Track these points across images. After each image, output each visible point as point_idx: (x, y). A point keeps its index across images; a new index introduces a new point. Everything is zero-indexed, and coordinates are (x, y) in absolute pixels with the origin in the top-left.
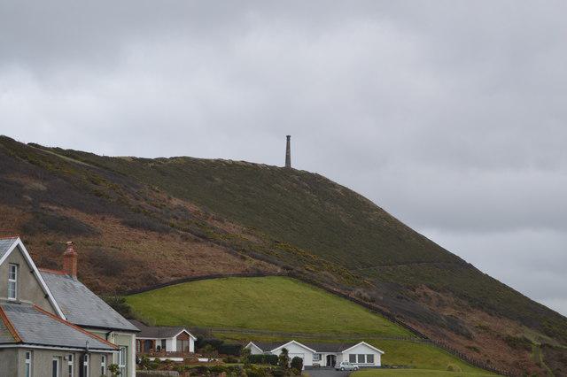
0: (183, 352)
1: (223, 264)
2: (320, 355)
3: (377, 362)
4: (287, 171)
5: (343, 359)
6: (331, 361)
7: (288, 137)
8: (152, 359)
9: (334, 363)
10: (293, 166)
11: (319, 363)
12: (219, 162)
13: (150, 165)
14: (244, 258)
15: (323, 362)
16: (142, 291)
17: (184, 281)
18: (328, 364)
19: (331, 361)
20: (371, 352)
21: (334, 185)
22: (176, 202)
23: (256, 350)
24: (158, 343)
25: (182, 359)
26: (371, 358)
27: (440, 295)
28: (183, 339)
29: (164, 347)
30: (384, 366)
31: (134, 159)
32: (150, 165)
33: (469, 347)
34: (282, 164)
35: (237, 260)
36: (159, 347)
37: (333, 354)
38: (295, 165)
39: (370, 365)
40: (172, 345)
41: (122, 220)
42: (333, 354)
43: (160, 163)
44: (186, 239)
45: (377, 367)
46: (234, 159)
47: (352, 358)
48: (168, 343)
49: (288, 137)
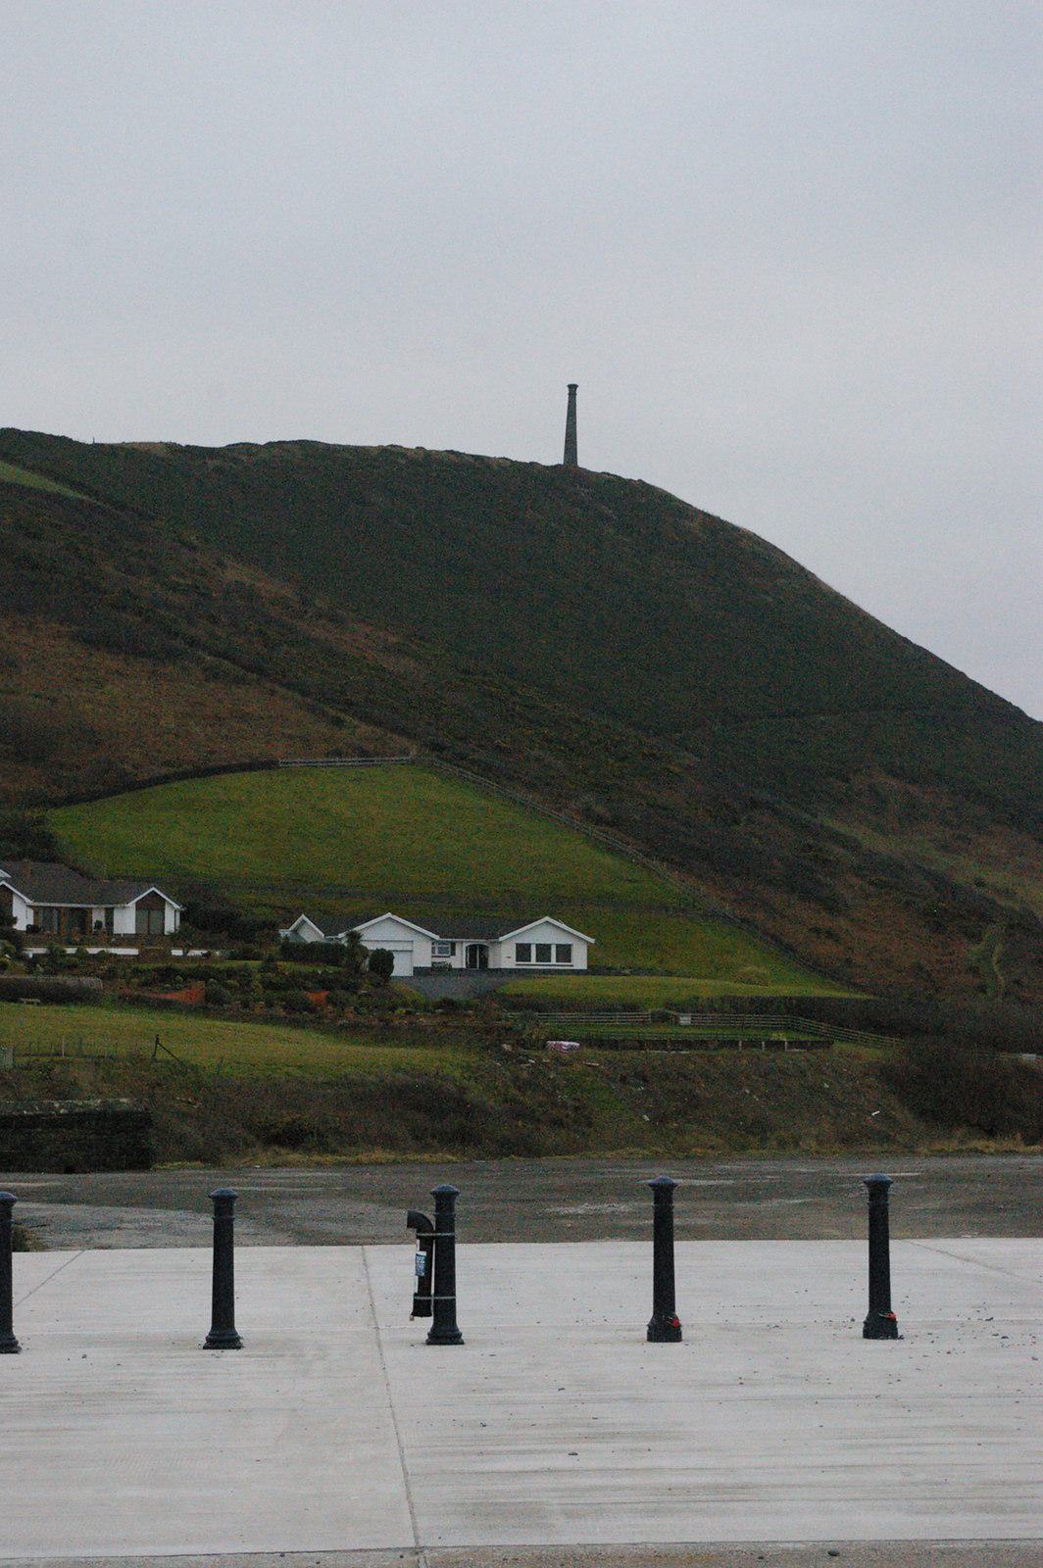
0: (148, 936)
1: (290, 737)
2: (453, 945)
3: (580, 960)
4: (569, 473)
5: (504, 956)
6: (478, 957)
7: (573, 388)
8: (71, 950)
9: (484, 961)
10: (584, 462)
11: (448, 961)
12: (391, 455)
13: (211, 463)
14: (338, 722)
15: (459, 960)
16: (93, 797)
17: (184, 776)
18: (471, 963)
19: (478, 957)
20: (564, 940)
21: (683, 510)
22: (236, 573)
23: (311, 933)
24: (98, 916)
25: (134, 952)
26: (565, 952)
27: (913, 789)
28: (151, 907)
29: (110, 923)
30: (593, 969)
31: (172, 448)
32: (211, 463)
33: (817, 930)
34: (553, 456)
35: (323, 728)
36: (99, 924)
37: (482, 941)
38: (590, 460)
39: (563, 966)
40: (126, 921)
41: (74, 628)
42: (482, 941)
43: (235, 460)
44: (212, 674)
45: (578, 972)
46: (430, 446)
47: (523, 952)
48: (117, 916)
49: (573, 388)
